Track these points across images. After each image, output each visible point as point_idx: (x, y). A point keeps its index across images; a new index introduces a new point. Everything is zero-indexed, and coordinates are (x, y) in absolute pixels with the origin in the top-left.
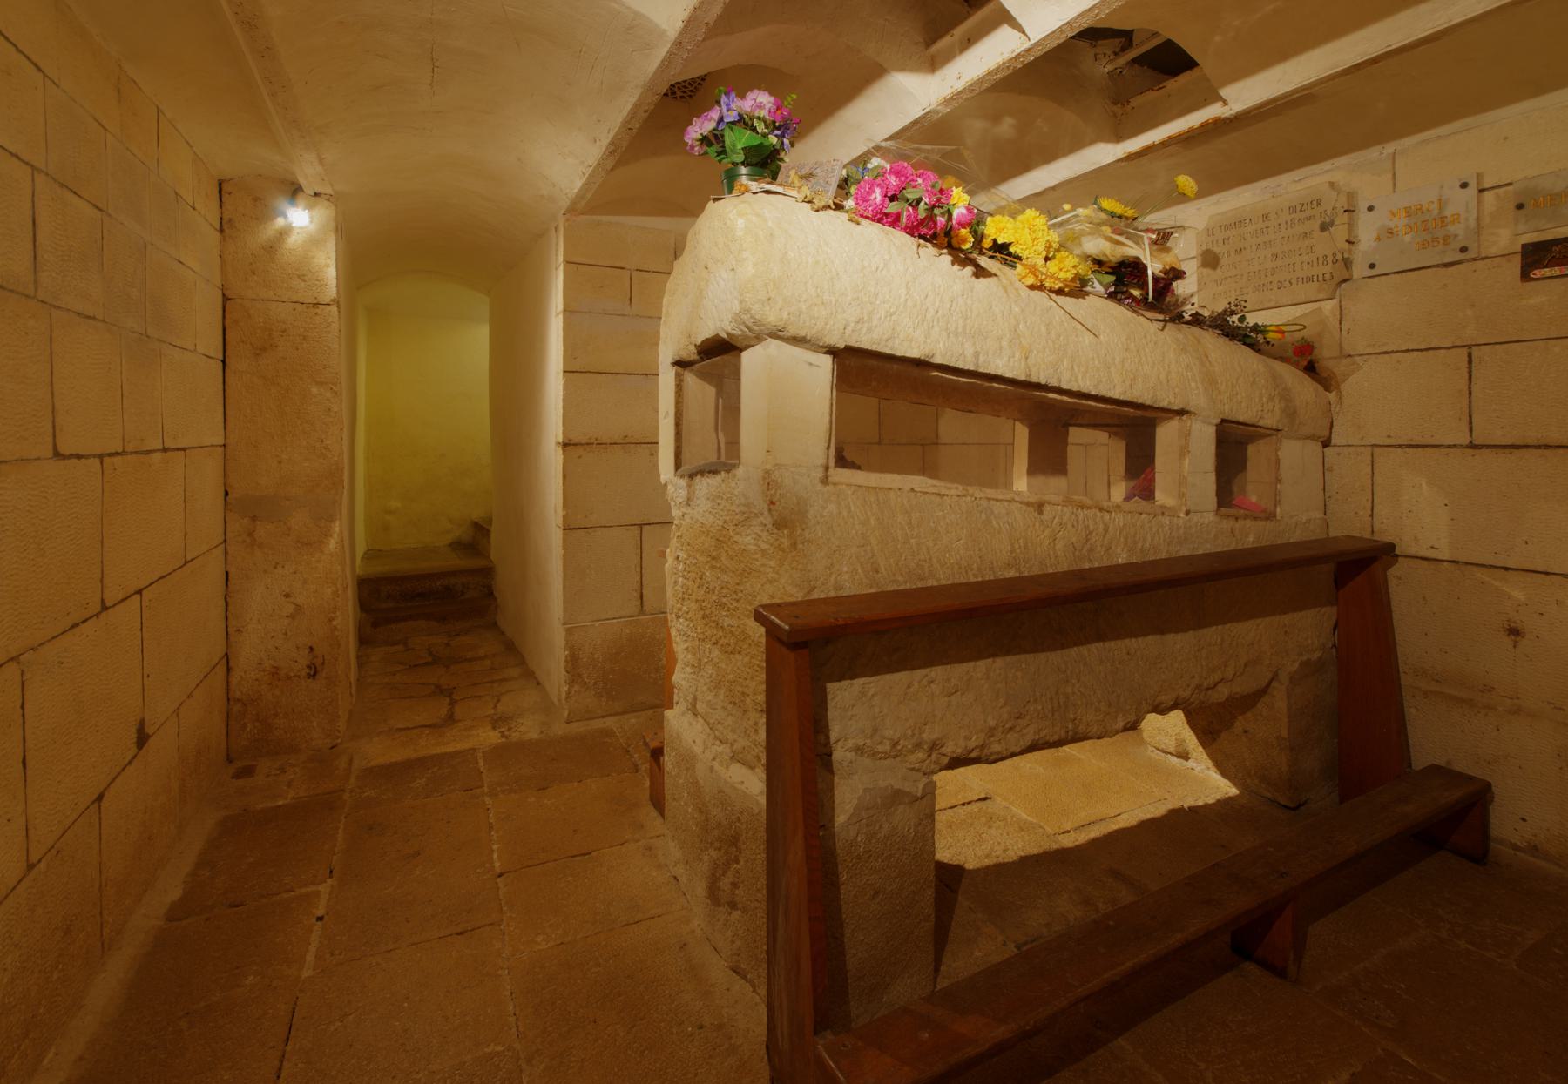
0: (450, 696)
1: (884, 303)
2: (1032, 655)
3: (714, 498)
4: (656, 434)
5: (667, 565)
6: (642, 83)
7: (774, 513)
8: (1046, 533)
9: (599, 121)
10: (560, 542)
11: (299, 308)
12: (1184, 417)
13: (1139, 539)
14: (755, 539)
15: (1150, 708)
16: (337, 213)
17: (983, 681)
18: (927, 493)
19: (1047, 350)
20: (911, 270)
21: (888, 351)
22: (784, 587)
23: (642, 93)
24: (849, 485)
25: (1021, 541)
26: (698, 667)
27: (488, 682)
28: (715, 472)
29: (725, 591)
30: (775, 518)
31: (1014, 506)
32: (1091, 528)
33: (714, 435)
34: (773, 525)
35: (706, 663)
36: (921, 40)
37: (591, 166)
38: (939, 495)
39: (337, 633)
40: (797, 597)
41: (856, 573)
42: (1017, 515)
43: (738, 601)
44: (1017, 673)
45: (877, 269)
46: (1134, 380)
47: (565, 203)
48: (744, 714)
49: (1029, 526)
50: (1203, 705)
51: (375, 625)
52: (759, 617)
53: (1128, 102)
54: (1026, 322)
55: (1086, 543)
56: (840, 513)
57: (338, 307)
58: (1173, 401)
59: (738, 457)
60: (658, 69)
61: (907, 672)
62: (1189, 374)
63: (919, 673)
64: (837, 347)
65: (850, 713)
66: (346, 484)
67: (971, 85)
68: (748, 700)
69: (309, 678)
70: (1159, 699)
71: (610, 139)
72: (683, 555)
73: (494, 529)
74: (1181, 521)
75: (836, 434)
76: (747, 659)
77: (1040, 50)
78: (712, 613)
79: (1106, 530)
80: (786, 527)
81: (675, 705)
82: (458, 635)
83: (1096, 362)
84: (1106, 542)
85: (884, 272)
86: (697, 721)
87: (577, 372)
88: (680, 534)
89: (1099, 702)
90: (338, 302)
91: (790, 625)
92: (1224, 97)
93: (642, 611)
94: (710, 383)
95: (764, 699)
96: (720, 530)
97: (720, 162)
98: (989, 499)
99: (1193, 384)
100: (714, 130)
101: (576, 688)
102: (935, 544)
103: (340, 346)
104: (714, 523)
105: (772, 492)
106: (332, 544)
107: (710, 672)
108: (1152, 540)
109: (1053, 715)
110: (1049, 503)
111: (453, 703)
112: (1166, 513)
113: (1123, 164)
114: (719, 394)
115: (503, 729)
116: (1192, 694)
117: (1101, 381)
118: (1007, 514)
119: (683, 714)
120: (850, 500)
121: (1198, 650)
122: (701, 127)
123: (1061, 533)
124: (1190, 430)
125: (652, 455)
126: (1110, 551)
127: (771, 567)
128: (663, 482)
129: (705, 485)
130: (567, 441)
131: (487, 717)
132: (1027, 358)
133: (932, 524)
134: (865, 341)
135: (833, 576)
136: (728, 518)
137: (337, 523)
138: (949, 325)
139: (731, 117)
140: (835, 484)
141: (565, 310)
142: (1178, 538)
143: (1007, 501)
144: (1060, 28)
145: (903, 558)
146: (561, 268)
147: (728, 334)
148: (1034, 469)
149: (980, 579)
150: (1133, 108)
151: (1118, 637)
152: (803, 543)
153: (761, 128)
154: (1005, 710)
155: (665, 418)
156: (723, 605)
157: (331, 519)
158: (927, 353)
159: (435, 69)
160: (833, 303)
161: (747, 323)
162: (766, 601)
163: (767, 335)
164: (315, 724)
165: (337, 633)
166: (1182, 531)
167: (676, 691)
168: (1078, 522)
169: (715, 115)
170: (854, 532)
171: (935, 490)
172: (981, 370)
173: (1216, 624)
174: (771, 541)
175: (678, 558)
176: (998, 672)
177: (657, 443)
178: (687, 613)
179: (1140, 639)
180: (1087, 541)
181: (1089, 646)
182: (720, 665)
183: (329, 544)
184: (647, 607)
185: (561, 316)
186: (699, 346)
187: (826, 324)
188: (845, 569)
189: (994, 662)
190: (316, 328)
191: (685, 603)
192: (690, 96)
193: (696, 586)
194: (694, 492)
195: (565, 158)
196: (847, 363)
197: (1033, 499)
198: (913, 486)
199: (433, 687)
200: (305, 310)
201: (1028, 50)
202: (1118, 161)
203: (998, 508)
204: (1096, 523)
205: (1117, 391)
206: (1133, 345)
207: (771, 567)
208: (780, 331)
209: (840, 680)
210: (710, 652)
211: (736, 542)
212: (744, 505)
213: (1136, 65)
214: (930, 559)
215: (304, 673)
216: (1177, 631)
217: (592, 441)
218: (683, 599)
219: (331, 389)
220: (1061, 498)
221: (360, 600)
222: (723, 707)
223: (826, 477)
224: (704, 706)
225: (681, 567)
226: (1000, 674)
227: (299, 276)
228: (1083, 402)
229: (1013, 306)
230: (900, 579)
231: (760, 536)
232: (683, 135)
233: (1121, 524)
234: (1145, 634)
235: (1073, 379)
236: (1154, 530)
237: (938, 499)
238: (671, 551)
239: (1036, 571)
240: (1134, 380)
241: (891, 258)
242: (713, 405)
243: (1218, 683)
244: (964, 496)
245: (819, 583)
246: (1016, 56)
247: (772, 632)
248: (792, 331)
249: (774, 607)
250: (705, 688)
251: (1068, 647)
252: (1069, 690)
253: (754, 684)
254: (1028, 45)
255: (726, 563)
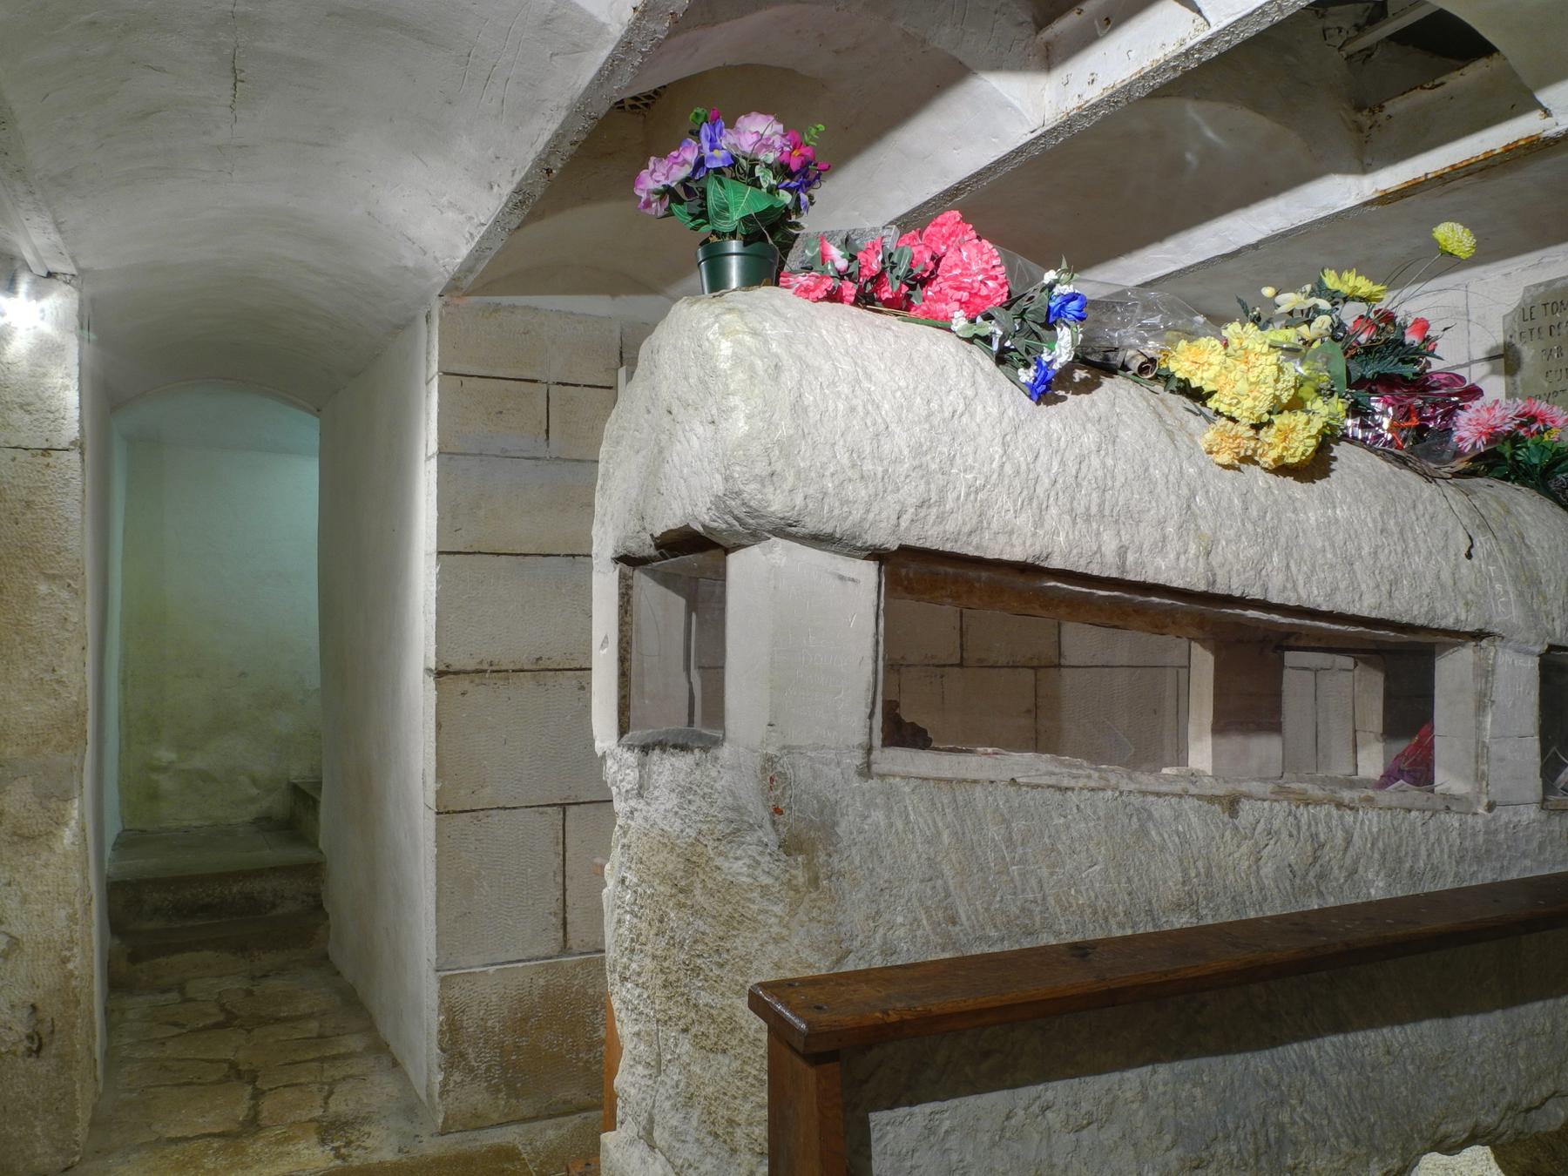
0: (253, 1081)
1: (965, 471)
2: (1220, 1059)
3: (685, 791)
4: (588, 654)
5: (605, 891)
6: (567, 103)
7: (781, 828)
8: (1244, 849)
9: (497, 158)
10: (431, 834)
11: (21, 456)
12: (1484, 643)
13: (1407, 854)
14: (749, 866)
15: (1428, 1146)
16: (81, 301)
17: (1135, 1106)
18: (1038, 786)
19: (1243, 538)
20: (1010, 412)
21: (971, 551)
22: (797, 952)
23: (567, 117)
24: (906, 777)
25: (1200, 864)
26: (657, 1067)
27: (313, 1060)
28: (684, 748)
29: (700, 947)
30: (783, 836)
31: (1188, 804)
32: (1322, 837)
33: (683, 675)
34: (780, 847)
35: (670, 1061)
36: (1029, 19)
37: (483, 225)
38: (1060, 789)
39: (74, 983)
40: (819, 969)
41: (919, 926)
42: (1194, 820)
43: (721, 966)
44: (1194, 1090)
45: (954, 412)
46: (1394, 583)
47: (441, 279)
48: (731, 1156)
49: (1214, 838)
50: (1521, 1137)
51: (134, 958)
52: (756, 1004)
53: (1381, 107)
54: (1207, 492)
55: (1312, 864)
56: (891, 825)
57: (82, 454)
58: (1463, 617)
59: (722, 727)
60: (592, 82)
61: (1005, 1092)
62: (1491, 568)
63: (1026, 1093)
64: (886, 549)
65: (908, 1164)
66: (90, 736)
67: (1111, 96)
68: (739, 1133)
69: (30, 1056)
70: (1443, 1129)
71: (514, 185)
72: (632, 878)
73: (324, 799)
74: (1480, 821)
75: (883, 691)
76: (736, 1064)
77: (1227, 42)
78: (679, 980)
79: (1348, 841)
80: (800, 850)
81: (618, 1125)
82: (265, 976)
83: (1329, 556)
84: (1348, 861)
85: (964, 419)
86: (655, 1158)
87: (459, 553)
88: (625, 841)
89: (1338, 1137)
90: (82, 444)
91: (808, 1024)
92: (1545, 105)
93: (565, 949)
94: (677, 592)
95: (765, 1134)
96: (692, 845)
97: (695, 229)
98: (1144, 793)
99: (1498, 586)
100: (688, 179)
101: (457, 1077)
102: (1052, 874)
103: (83, 514)
104: (682, 831)
105: (778, 792)
106: (68, 836)
107: (675, 1077)
108: (1429, 855)
109: (1257, 1161)
110: (1249, 797)
111: (257, 1095)
112: (1454, 808)
113: (1374, 209)
114: (691, 607)
115: (336, 1144)
116: (1503, 1119)
117: (1337, 588)
118: (1176, 818)
119: (632, 1142)
120: (908, 801)
121: (1512, 1044)
122: (660, 175)
123: (1269, 847)
124: (1494, 665)
125: (582, 688)
126: (1356, 877)
127: (776, 916)
128: (600, 754)
129: (668, 765)
130: (442, 668)
131: (311, 1121)
132: (1208, 554)
133: (1047, 840)
134: (933, 536)
135: (881, 931)
136: (704, 827)
137: (76, 803)
138: (1075, 504)
139: (717, 159)
140: (882, 776)
141: (440, 452)
142: (1474, 850)
143: (1174, 795)
144: (1260, 7)
145: (998, 899)
146: (435, 382)
147: (704, 526)
148: (1224, 724)
149: (1129, 932)
150: (1390, 117)
151: (1371, 1024)
152: (829, 878)
153: (767, 179)
154: (1174, 1153)
155: (602, 647)
156: (697, 971)
157: (66, 798)
158: (1037, 553)
159: (239, 84)
160: (880, 475)
161: (736, 512)
162: (770, 976)
163: (769, 532)
164: (38, 1130)
165: (74, 983)
166: (1481, 839)
167: (620, 1103)
168: (1299, 829)
169: (691, 156)
170: (914, 856)
171: (1052, 781)
172: (1131, 577)
173: (1541, 997)
174: (778, 872)
175: (623, 881)
176: (1161, 1088)
177: (590, 669)
178: (639, 974)
179: (1408, 1028)
180: (1316, 859)
181: (1319, 1041)
182: (692, 1067)
183: (62, 837)
184: (574, 942)
185: (434, 462)
186: (657, 538)
187: (868, 511)
188: (900, 919)
189: (1154, 1072)
190: (45, 488)
191: (635, 957)
192: (646, 105)
193: (653, 932)
194: (649, 777)
195: (442, 213)
196: (903, 572)
197: (1221, 790)
198: (1015, 776)
199: (225, 1066)
200: (30, 459)
201: (1208, 42)
202: (1366, 204)
203: (1161, 808)
204: (1330, 829)
205: (1365, 604)
206: (1392, 522)
207: (776, 916)
208: (791, 526)
209: (890, 1108)
210: (676, 1045)
211: (718, 868)
212: (733, 809)
213: (1393, 43)
214: (1044, 899)
215: (21, 1048)
216: (1474, 1010)
217: (485, 667)
218: (632, 951)
219: (69, 585)
220: (1270, 787)
221: (110, 917)
222: (697, 1140)
223: (868, 765)
224: (666, 1135)
225: (628, 897)
226: (1164, 1093)
227: (21, 407)
228: (1308, 622)
229: (1185, 465)
230: (993, 933)
231: (758, 863)
232: (634, 186)
233: (1375, 830)
234: (1417, 1018)
235: (1289, 586)
236: (1432, 838)
237: (1058, 796)
238: (612, 867)
239: (1226, 916)
240: (1394, 583)
241: (977, 394)
242: (682, 625)
243: (1547, 1099)
244: (1103, 790)
245: (857, 943)
246: (1187, 51)
247: (779, 1030)
248: (810, 525)
249: (779, 988)
250: (667, 1105)
251: (1283, 1043)
252: (1285, 1117)
253: (748, 1106)
254: (1206, 34)
255: (701, 899)
